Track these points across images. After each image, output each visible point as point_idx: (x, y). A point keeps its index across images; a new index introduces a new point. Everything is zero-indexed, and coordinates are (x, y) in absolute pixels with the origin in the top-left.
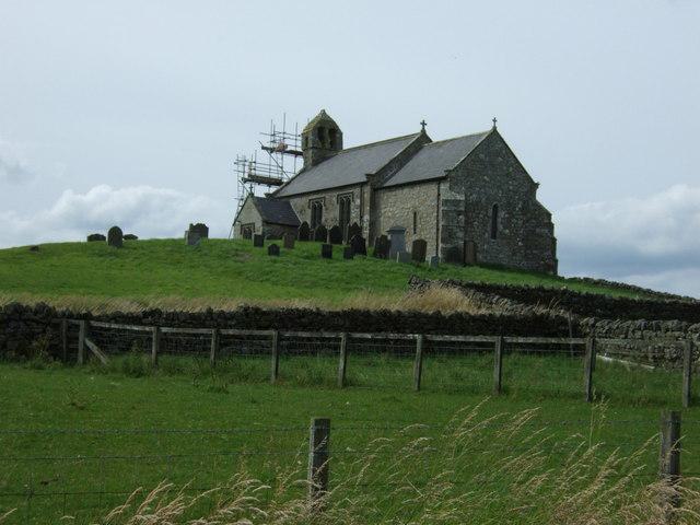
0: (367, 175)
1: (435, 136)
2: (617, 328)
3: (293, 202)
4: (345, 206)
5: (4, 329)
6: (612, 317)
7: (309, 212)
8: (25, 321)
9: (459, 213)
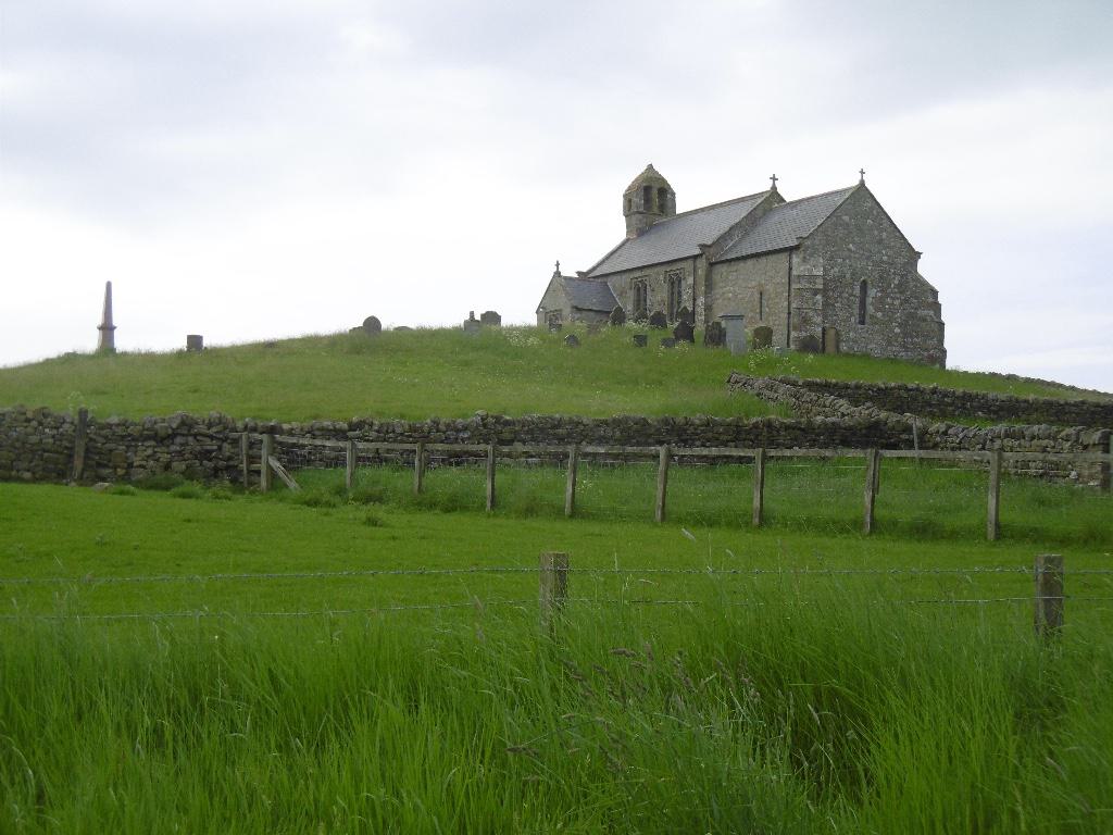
0: (699, 245)
1: (789, 194)
2: (975, 435)
3: (610, 282)
4: (675, 283)
5: (168, 446)
6: (1000, 419)
7: (631, 295)
8: (195, 436)
9: (816, 292)
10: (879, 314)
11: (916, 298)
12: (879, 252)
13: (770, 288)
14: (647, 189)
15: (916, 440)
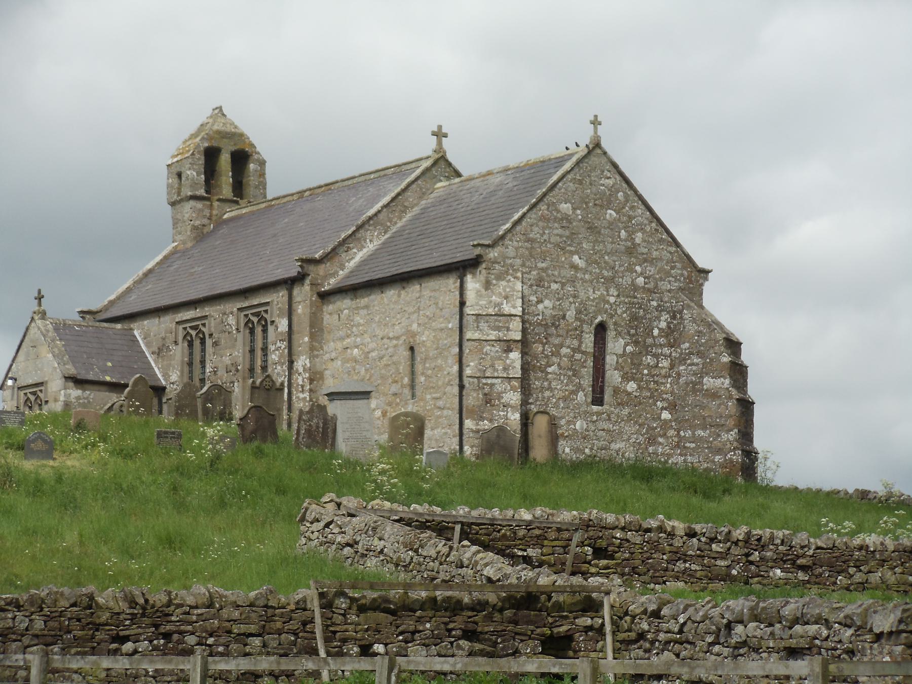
7: (178, 352)
10: (632, 386)
11: (700, 354)
12: (631, 270)
13: (425, 337)
14: (211, 155)
15: (608, 628)
